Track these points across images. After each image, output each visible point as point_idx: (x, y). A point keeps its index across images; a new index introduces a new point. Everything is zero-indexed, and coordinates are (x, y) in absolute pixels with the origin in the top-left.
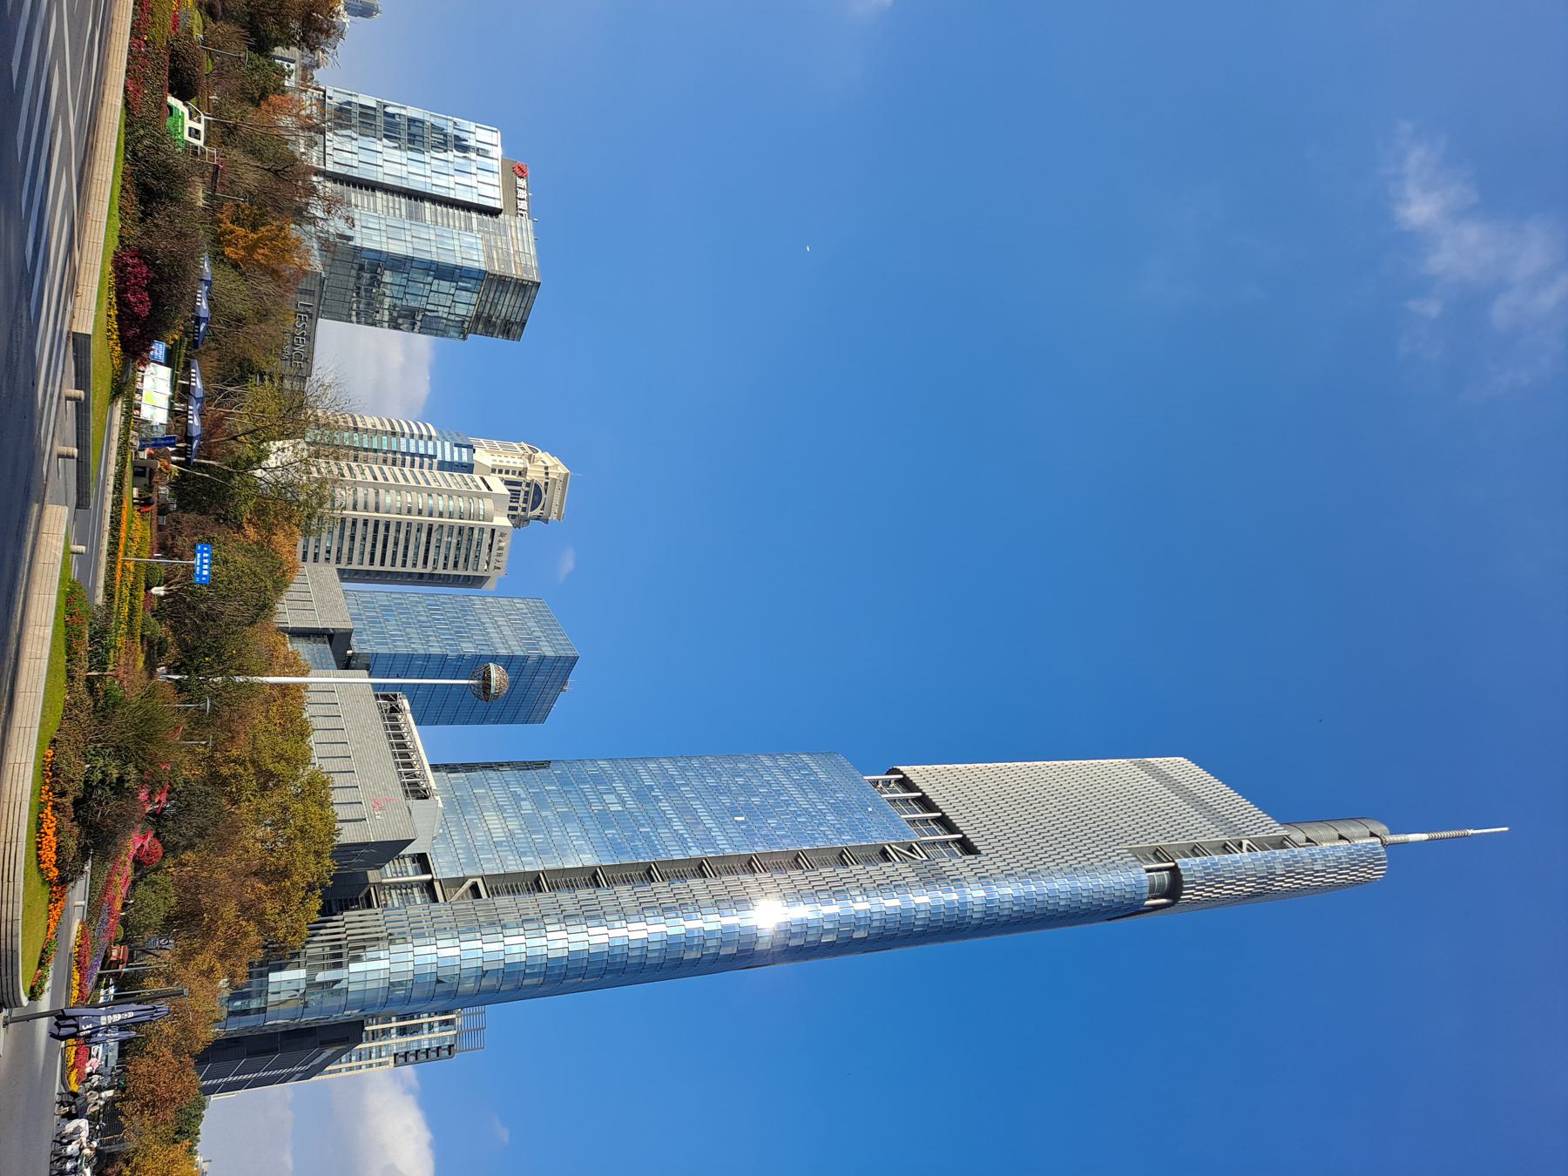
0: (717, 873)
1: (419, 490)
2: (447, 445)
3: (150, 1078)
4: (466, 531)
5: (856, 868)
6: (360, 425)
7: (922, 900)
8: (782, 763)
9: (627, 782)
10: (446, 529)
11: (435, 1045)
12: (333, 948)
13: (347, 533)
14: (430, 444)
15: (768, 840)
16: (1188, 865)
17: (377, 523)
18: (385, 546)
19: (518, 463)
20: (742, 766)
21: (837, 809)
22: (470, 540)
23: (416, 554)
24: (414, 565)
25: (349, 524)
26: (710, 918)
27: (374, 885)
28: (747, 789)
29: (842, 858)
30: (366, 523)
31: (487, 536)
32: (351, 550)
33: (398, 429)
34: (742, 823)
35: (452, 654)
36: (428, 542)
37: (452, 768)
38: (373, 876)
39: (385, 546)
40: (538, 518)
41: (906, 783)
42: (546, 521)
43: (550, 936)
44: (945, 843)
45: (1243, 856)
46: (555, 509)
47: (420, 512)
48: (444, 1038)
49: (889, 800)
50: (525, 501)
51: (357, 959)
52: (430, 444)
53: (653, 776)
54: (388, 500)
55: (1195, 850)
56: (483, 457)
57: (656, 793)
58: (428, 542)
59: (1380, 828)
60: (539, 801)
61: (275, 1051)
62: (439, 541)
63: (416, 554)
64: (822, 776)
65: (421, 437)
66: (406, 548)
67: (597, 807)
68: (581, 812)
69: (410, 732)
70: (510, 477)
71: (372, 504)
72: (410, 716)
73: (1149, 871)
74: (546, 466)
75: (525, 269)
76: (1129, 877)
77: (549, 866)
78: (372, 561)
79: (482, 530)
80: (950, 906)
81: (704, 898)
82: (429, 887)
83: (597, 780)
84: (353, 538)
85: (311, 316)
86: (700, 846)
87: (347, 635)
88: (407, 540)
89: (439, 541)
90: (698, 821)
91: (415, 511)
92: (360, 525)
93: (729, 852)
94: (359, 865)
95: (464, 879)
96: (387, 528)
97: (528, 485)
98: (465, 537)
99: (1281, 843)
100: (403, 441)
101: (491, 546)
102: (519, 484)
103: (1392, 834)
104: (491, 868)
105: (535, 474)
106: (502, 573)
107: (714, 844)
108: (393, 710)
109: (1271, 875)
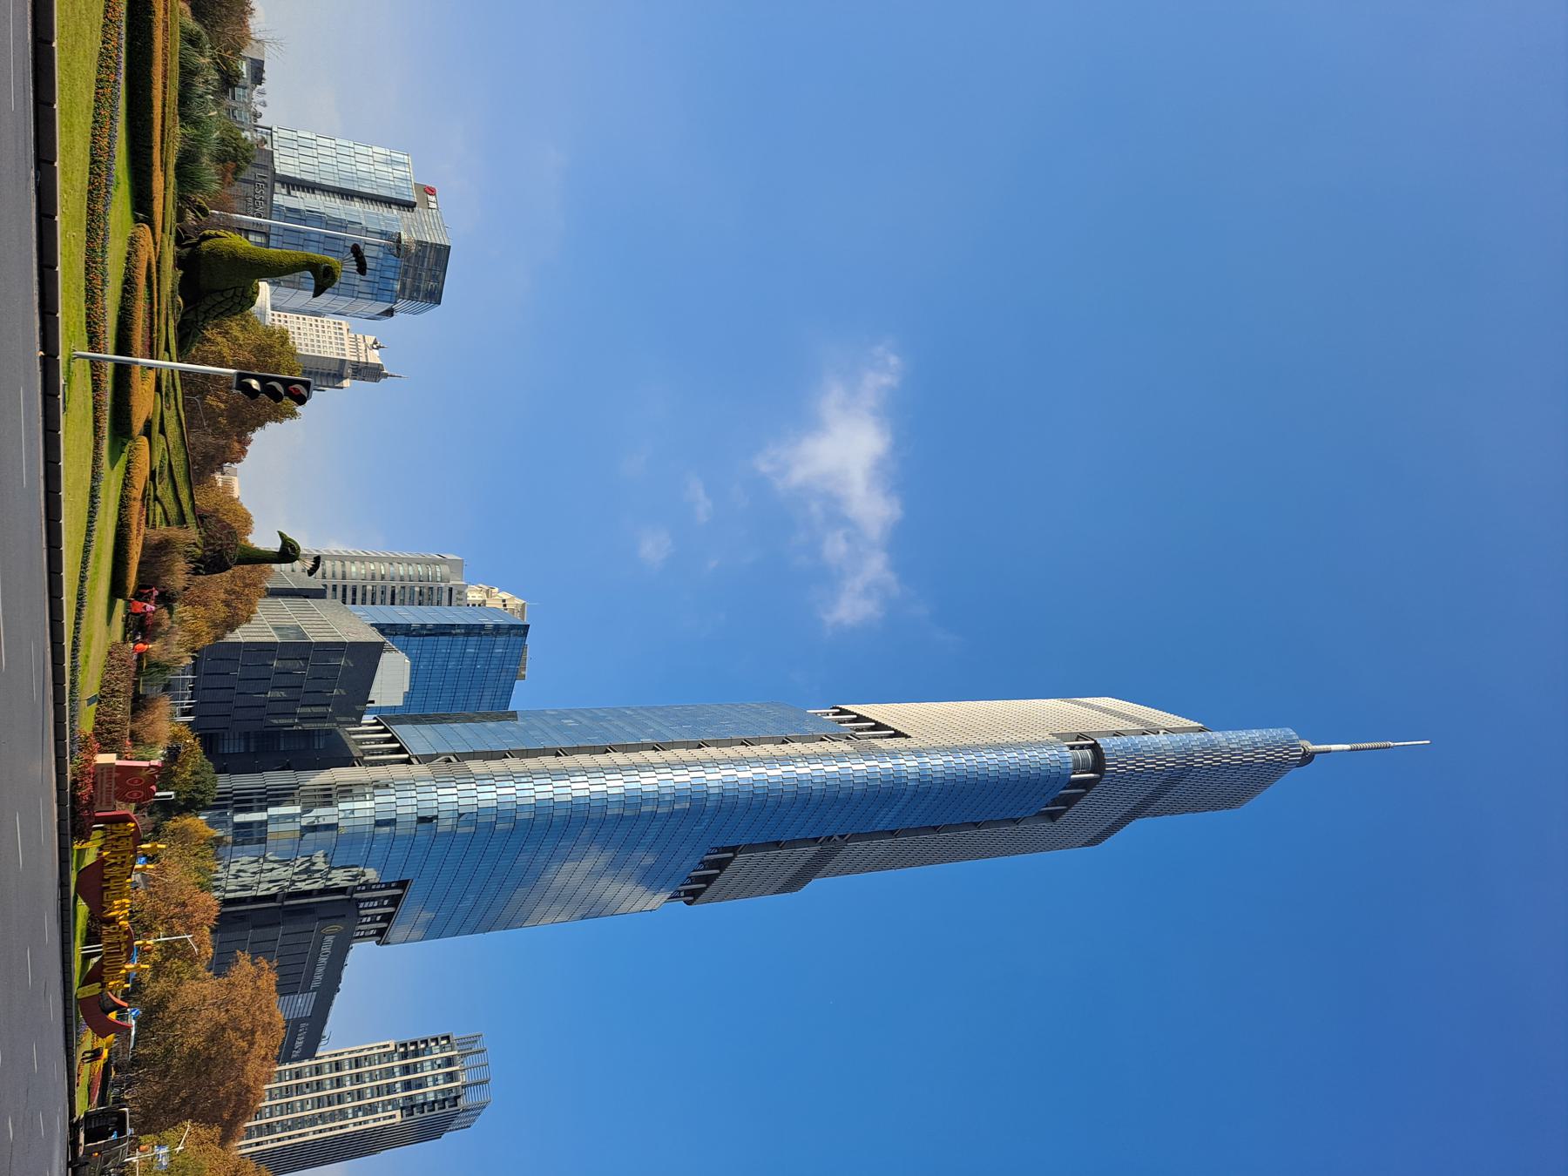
11: (440, 1097)
16: (1104, 742)
17: (345, 588)
41: (843, 712)
48: (450, 1090)
73: (1072, 748)
80: (886, 774)
91: (378, 576)
95: (438, 756)
96: (354, 593)
109: (1188, 753)
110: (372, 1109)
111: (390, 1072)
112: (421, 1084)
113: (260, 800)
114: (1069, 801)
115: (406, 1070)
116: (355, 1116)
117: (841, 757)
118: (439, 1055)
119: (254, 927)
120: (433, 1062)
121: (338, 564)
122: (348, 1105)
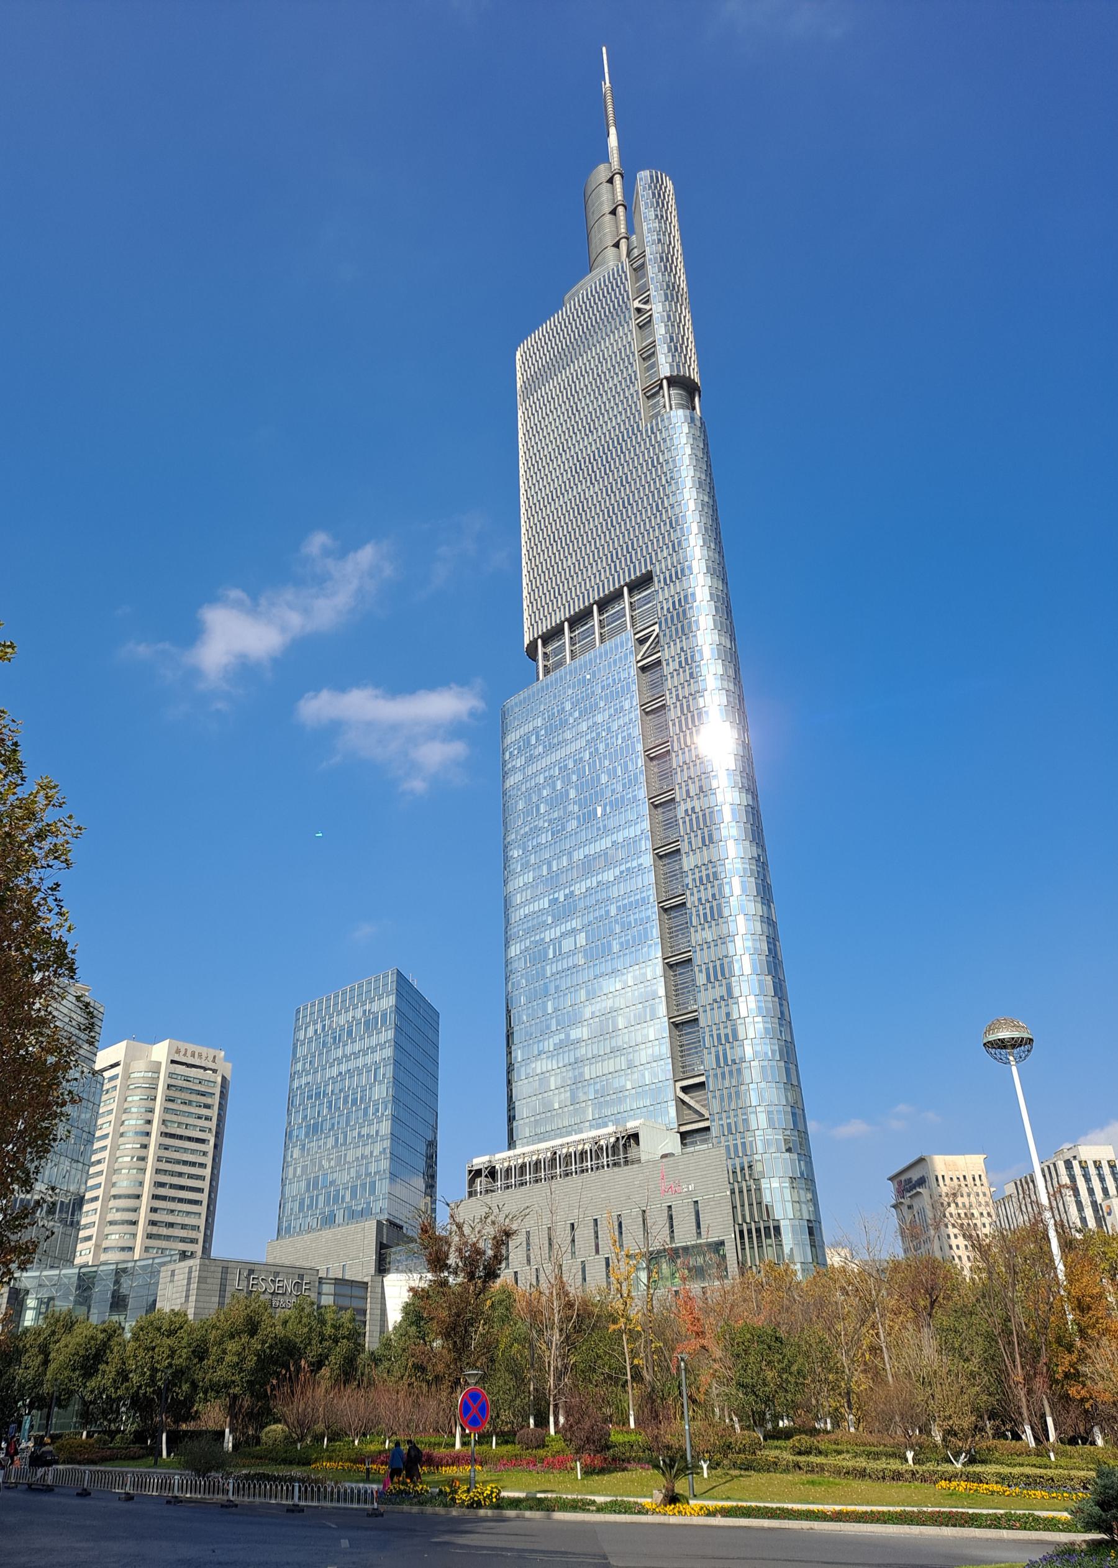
4: (172, 1093)
9: (544, 926)
12: (768, 1236)
13: (164, 1231)
15: (632, 782)
17: (155, 1197)
18: (182, 1188)
21: (589, 711)
22: (182, 1089)
23: (193, 1151)
24: (205, 1154)
25: (155, 1230)
32: (184, 1227)
34: (605, 810)
39: (182, 1188)
53: (534, 899)
55: (648, 355)
59: (602, 172)
63: (193, 1151)
64: (539, 722)
66: (185, 1163)
71: (131, 1203)
73: (671, 408)
78: (197, 1202)
79: (171, 1075)
84: (171, 1225)
85: (251, 1272)
86: (638, 854)
90: (604, 853)
92: (156, 1217)
98: (177, 1094)
103: (606, 159)
104: (665, 1069)
107: (636, 840)
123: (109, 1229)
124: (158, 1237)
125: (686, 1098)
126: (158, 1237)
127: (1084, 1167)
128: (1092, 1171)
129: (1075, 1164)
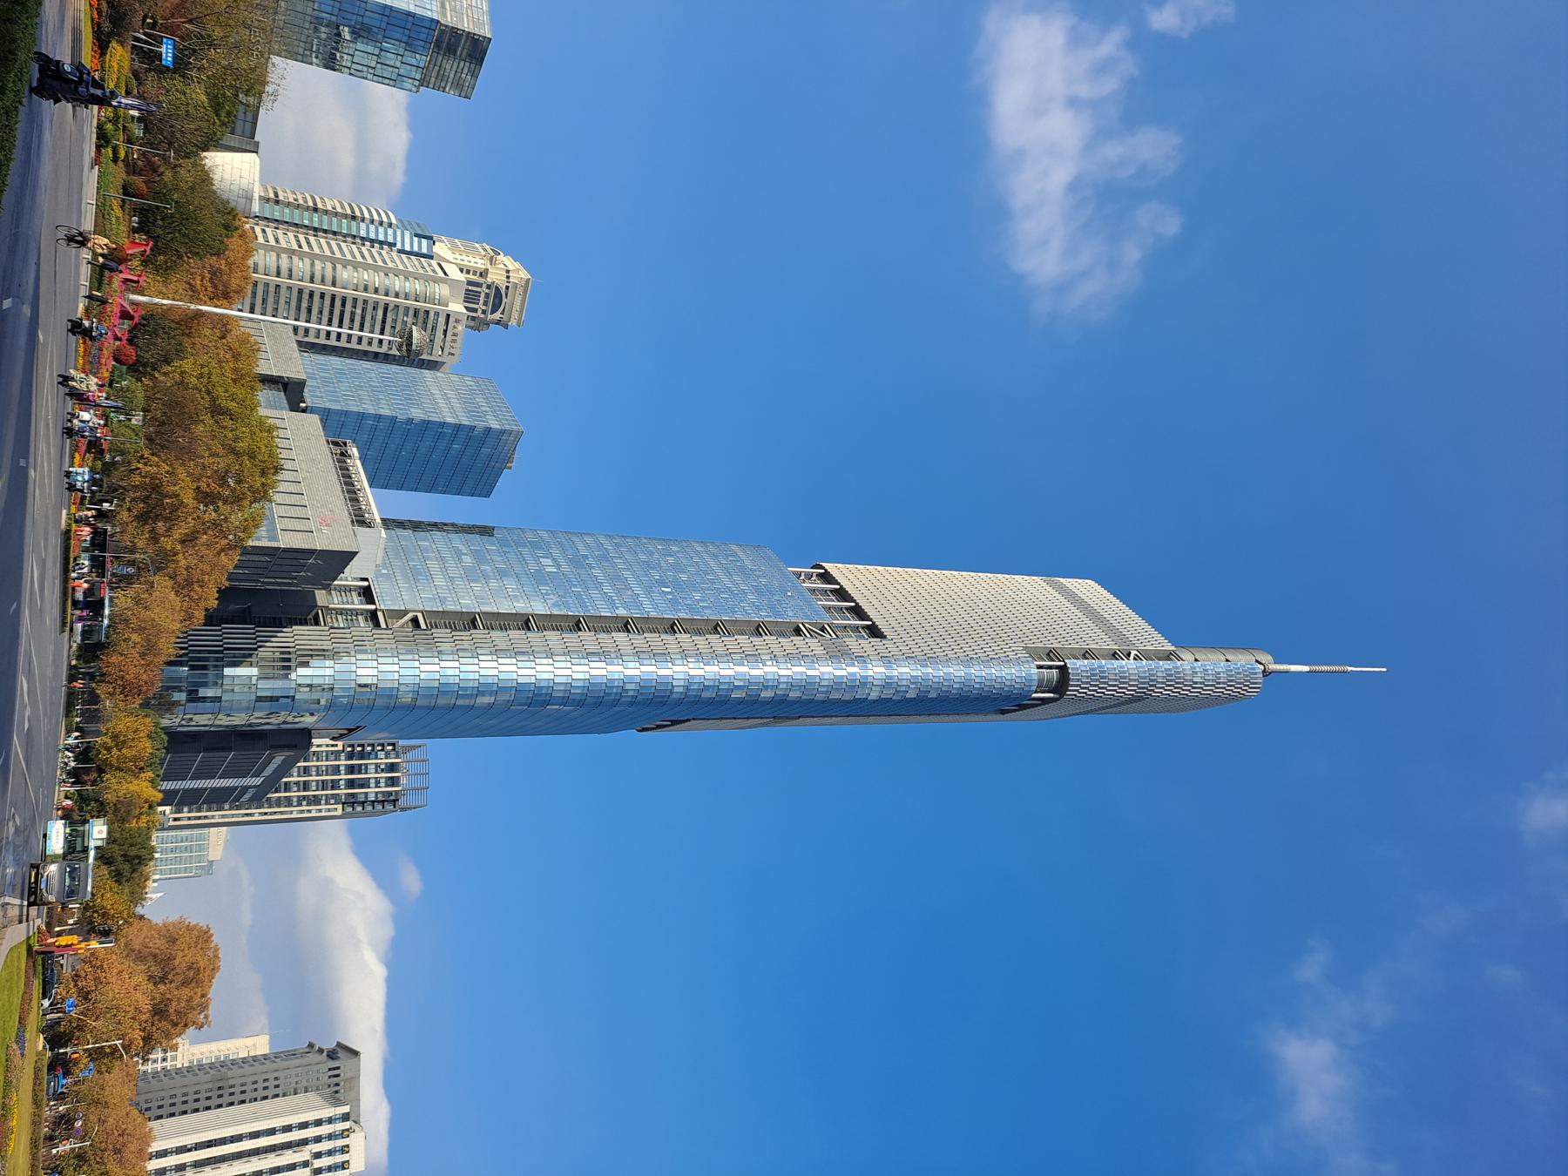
0: (641, 631)
1: (376, 269)
2: (407, 235)
3: (120, 666)
4: (421, 315)
5: (769, 638)
6: (320, 206)
7: (827, 671)
8: (711, 548)
9: (564, 550)
10: (401, 310)
11: (380, 798)
13: (304, 305)
14: (390, 231)
16: (1076, 665)
17: (333, 297)
19: (479, 263)
20: (675, 549)
21: (758, 590)
25: (306, 296)
26: (631, 665)
27: (321, 608)
28: (677, 568)
29: (758, 630)
30: (322, 296)
31: (442, 320)
33: (358, 213)
35: (401, 417)
36: (384, 322)
37: (401, 524)
38: (321, 597)
40: (498, 322)
41: (826, 577)
42: (506, 326)
43: (482, 664)
44: (856, 629)
45: (1129, 665)
46: (515, 315)
47: (376, 291)
48: (390, 793)
49: (824, 607)
50: (485, 303)
51: (306, 664)
52: (390, 231)
54: (345, 275)
55: (1086, 654)
56: (440, 248)
57: (590, 561)
58: (384, 322)
59: (1266, 658)
60: (479, 557)
61: (230, 749)
62: (395, 321)
65: (381, 223)
67: (533, 567)
68: (518, 569)
69: (365, 496)
70: (471, 276)
71: (329, 278)
72: (358, 463)
73: (1040, 667)
74: (507, 269)
75: (480, 24)
76: (1022, 672)
77: (485, 609)
79: (437, 314)
81: (626, 648)
82: (373, 616)
83: (535, 546)
87: (301, 384)
88: (363, 318)
89: (395, 321)
91: (371, 289)
92: (316, 298)
93: (653, 614)
94: (306, 580)
95: (405, 612)
96: (343, 304)
97: (489, 287)
99: (1168, 656)
100: (363, 225)
101: (445, 332)
102: (480, 285)
105: (497, 277)
106: (455, 359)
108: (342, 454)
109: (1152, 682)
110: (316, 801)
111: (336, 770)
112: (364, 784)
113: (217, 659)
114: (1022, 707)
115: (351, 784)
116: (300, 804)
117: (814, 659)
118: (383, 761)
119: (206, 750)
120: (377, 766)
121: (329, 265)
122: (294, 794)
123: (307, 261)
124: (300, 300)
125: (407, 618)
126: (300, 300)
127: (343, 1134)
128: (340, 1143)
129: (347, 1125)
